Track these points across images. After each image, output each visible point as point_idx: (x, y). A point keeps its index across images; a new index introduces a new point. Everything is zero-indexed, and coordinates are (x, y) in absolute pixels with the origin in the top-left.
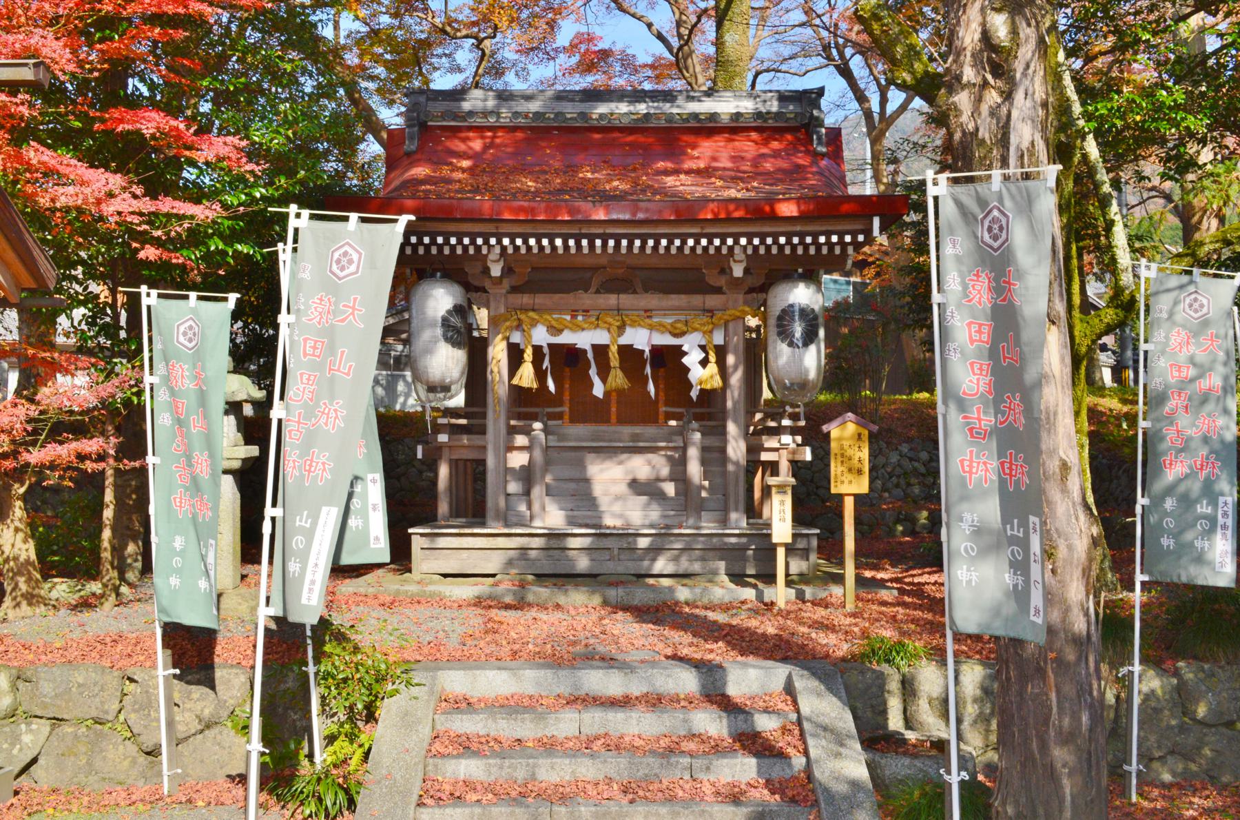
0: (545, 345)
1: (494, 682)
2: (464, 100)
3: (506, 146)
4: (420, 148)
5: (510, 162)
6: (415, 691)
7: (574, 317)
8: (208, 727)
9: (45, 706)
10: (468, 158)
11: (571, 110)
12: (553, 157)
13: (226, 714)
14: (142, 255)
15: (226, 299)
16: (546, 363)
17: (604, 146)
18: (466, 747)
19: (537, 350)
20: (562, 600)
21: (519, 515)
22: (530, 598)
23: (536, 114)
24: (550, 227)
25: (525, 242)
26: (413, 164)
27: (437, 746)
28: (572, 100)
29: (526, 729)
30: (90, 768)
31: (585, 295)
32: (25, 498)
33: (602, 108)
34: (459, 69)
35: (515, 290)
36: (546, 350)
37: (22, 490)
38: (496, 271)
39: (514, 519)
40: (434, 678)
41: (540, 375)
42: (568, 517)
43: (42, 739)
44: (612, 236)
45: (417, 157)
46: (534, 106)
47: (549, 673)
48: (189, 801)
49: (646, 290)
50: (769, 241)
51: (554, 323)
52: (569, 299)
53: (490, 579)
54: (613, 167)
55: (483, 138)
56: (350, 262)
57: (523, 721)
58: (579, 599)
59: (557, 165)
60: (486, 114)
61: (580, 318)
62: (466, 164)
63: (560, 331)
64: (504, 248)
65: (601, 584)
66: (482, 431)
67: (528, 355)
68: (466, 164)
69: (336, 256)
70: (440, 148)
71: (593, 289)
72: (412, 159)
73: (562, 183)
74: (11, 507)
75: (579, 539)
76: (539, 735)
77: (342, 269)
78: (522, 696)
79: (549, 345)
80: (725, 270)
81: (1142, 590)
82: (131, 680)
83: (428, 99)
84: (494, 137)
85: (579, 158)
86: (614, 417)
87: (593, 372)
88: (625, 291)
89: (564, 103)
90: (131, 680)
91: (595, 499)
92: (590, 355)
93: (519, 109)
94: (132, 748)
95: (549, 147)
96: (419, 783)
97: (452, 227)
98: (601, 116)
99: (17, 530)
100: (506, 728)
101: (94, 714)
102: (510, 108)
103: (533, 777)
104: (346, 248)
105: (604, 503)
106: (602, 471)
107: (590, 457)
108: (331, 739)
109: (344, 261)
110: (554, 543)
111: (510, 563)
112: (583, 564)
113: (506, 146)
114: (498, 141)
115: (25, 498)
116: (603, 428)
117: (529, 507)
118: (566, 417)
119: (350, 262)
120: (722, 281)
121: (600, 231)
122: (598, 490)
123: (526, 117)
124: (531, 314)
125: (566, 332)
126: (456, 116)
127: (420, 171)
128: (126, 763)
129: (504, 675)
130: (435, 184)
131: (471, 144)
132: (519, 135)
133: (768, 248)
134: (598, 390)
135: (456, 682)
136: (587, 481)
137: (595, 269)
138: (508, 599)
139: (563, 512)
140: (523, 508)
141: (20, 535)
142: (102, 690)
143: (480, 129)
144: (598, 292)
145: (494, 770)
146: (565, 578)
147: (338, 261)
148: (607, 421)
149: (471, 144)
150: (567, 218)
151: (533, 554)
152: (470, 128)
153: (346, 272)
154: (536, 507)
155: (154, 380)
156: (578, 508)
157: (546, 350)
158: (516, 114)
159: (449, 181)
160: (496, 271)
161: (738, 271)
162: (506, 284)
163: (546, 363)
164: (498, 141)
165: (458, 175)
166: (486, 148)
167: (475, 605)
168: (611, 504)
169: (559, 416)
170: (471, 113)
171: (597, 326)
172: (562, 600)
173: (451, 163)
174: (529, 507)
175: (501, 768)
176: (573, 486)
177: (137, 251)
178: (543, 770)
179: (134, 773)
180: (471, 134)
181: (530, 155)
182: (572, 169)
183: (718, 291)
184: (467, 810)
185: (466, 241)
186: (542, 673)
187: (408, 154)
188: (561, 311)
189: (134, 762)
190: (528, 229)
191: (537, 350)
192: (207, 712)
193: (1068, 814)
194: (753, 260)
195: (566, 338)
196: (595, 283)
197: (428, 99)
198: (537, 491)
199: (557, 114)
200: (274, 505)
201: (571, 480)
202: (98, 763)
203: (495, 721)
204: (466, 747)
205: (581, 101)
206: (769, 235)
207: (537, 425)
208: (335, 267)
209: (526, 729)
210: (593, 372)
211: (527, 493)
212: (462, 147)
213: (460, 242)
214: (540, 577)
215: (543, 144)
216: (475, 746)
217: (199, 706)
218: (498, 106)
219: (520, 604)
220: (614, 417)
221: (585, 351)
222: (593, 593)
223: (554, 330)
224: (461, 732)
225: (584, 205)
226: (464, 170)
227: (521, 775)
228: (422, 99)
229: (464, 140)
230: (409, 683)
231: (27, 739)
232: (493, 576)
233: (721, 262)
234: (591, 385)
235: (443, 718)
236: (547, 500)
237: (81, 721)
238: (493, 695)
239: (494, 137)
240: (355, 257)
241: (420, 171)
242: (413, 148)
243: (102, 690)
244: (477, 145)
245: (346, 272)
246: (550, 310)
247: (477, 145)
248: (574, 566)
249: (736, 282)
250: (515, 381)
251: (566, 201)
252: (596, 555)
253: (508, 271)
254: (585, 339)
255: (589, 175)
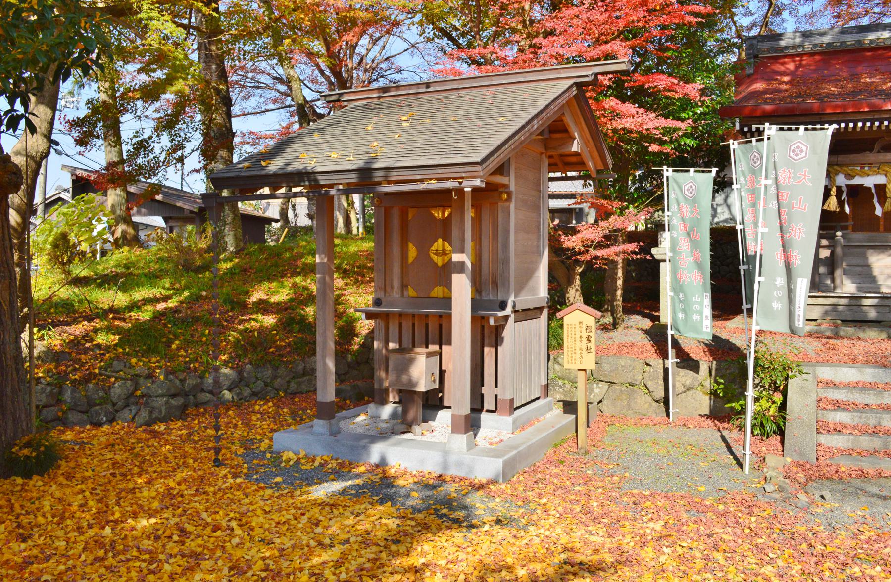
0: (844, 185)
1: (848, 374)
2: (781, 39)
3: (810, 65)
4: (756, 71)
5: (815, 76)
6: (805, 376)
7: (862, 168)
8: (688, 390)
9: (606, 376)
10: (787, 75)
11: (850, 39)
12: (841, 70)
13: (697, 384)
14: (650, 149)
15: (710, 171)
16: (844, 196)
17: (873, 59)
18: (838, 406)
19: (839, 189)
20: (861, 335)
21: (827, 286)
22: (842, 333)
23: (827, 44)
24: (857, 115)
26: (755, 81)
27: (821, 404)
28: (851, 33)
29: (871, 399)
30: (629, 407)
31: (871, 155)
32: (581, 274)
33: (872, 36)
34: (751, 14)
36: (845, 189)
37: (580, 270)
39: (824, 288)
40: (814, 370)
41: (841, 203)
42: (858, 287)
43: (604, 391)
45: (754, 77)
46: (826, 39)
47: (881, 371)
48: (684, 425)
51: (850, 172)
52: (860, 158)
53: (813, 322)
54: (883, 74)
55: (794, 61)
56: (802, 151)
57: (869, 395)
58: (872, 334)
59: (845, 75)
60: (795, 47)
61: (866, 168)
62: (786, 79)
63: (853, 177)
65: (884, 326)
67: (833, 191)
68: (786, 79)
69: (792, 148)
70: (768, 70)
71: (876, 150)
72: (751, 79)
73: (853, 87)
74: (574, 278)
75: (870, 300)
76: (879, 403)
77: (797, 155)
78: (864, 383)
79: (847, 185)
82: (648, 365)
83: (758, 41)
84: (801, 61)
85: (860, 69)
86: (881, 228)
87: (875, 201)
89: (846, 36)
90: (648, 365)
91: (875, 277)
92: (873, 190)
93: (817, 42)
94: (649, 399)
95: (838, 64)
96: (815, 424)
98: (871, 40)
99: (577, 290)
100: (859, 398)
101: (629, 381)
102: (810, 41)
103: (879, 424)
104: (799, 144)
105: (881, 280)
106: (878, 260)
107: (870, 252)
108: (757, 400)
109: (798, 151)
110: (854, 302)
111: (826, 313)
112: (872, 314)
113: (810, 65)
114: (804, 63)
115: (582, 275)
116: (875, 234)
117: (833, 281)
118: (850, 228)
119: (802, 151)
121: (887, 116)
122: (876, 272)
123: (821, 46)
124: (835, 167)
125: (857, 178)
126: (777, 50)
127: (759, 86)
128: (647, 406)
129: (854, 370)
130: (771, 93)
131: (788, 66)
132: (817, 58)
134: (878, 211)
135: (825, 373)
136: (868, 266)
138: (828, 333)
139: (854, 285)
140: (828, 282)
141: (578, 293)
142: (634, 368)
143: (792, 56)
144: (879, 152)
145: (856, 419)
146: (863, 323)
147: (794, 151)
148: (878, 230)
149: (788, 66)
150: (866, 110)
151: (840, 308)
152: (785, 57)
153: (800, 157)
154: (838, 281)
155: (669, 213)
156: (863, 282)
157: (845, 189)
158: (815, 45)
159: (779, 91)
163: (844, 196)
164: (804, 63)
165: (784, 87)
166: (797, 68)
167: (808, 336)
168: (885, 280)
170: (786, 47)
171: (878, 173)
172: (861, 335)
173: (777, 79)
174: (833, 281)
175: (860, 418)
176: (859, 269)
177: (648, 147)
178: (885, 420)
179: (651, 410)
180: (786, 60)
181: (827, 70)
182: (855, 77)
184: (846, 437)
186: (877, 370)
187: (749, 76)
188: (854, 165)
189: (651, 405)
191: (839, 189)
192: (688, 382)
195: (857, 181)
196: (877, 147)
197: (758, 41)
198: (838, 273)
199: (842, 43)
200: (760, 275)
201: (858, 266)
202: (633, 405)
203: (852, 394)
204: (838, 406)
205: (857, 33)
207: (839, 233)
208: (792, 154)
209: (871, 399)
210: (875, 201)
211: (831, 273)
212: (782, 68)
214: (845, 322)
215: (834, 62)
216: (842, 406)
217: (683, 379)
218: (803, 41)
219: (836, 336)
220: (881, 228)
221: (870, 188)
222: (881, 331)
223: (850, 176)
224: (834, 398)
225: (875, 101)
226: (786, 83)
227: (872, 422)
228: (755, 42)
229: (783, 64)
230: (801, 372)
231: (597, 391)
232: (815, 320)
234: (874, 208)
235: (822, 391)
236: (844, 277)
237: (622, 384)
238: (847, 381)
239: (801, 61)
240: (804, 149)
241: (759, 86)
242: (752, 71)
243: (634, 368)
244: (791, 66)
245: (800, 157)
246: (847, 165)
247: (791, 66)
248: (866, 316)
250: (825, 208)
251: (863, 99)
252: (880, 310)
254: (870, 181)
255: (868, 80)
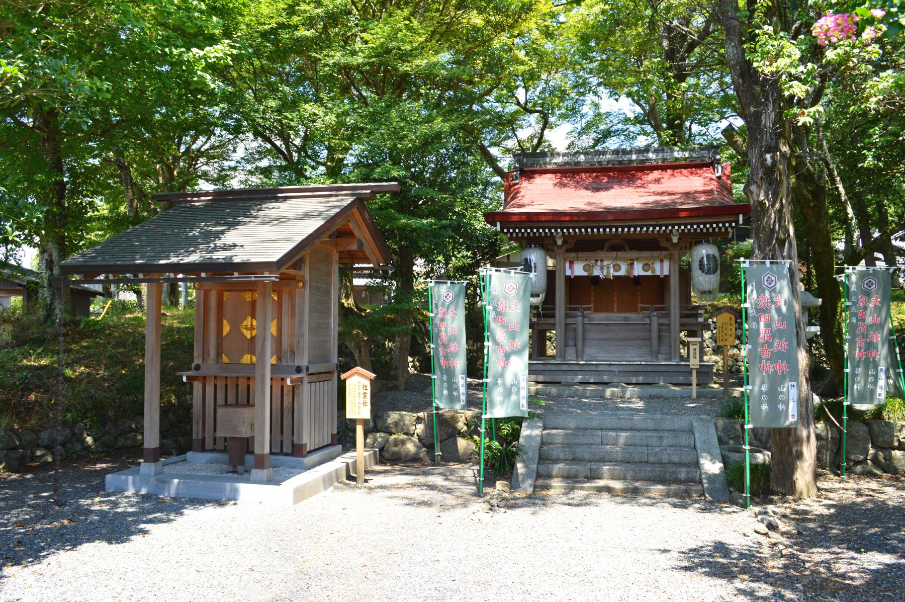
25: (544, 230)
35: (568, 251)
38: (560, 242)
44: (614, 227)
49: (631, 249)
50: (721, 225)
64: (563, 233)
66: (553, 316)
80: (669, 240)
81: (249, 376)
88: (620, 250)
97: (540, 225)
120: (667, 245)
133: (714, 229)
137: (607, 240)
160: (560, 242)
161: (675, 240)
162: (564, 248)
169: (589, 309)
183: (666, 249)
185: (708, 226)
190: (552, 225)
193: (903, 561)
194: (682, 235)
196: (607, 246)
206: (695, 224)
213: (526, 231)
233: (667, 237)
249: (675, 245)
253: (565, 242)
